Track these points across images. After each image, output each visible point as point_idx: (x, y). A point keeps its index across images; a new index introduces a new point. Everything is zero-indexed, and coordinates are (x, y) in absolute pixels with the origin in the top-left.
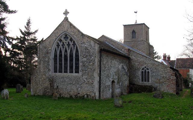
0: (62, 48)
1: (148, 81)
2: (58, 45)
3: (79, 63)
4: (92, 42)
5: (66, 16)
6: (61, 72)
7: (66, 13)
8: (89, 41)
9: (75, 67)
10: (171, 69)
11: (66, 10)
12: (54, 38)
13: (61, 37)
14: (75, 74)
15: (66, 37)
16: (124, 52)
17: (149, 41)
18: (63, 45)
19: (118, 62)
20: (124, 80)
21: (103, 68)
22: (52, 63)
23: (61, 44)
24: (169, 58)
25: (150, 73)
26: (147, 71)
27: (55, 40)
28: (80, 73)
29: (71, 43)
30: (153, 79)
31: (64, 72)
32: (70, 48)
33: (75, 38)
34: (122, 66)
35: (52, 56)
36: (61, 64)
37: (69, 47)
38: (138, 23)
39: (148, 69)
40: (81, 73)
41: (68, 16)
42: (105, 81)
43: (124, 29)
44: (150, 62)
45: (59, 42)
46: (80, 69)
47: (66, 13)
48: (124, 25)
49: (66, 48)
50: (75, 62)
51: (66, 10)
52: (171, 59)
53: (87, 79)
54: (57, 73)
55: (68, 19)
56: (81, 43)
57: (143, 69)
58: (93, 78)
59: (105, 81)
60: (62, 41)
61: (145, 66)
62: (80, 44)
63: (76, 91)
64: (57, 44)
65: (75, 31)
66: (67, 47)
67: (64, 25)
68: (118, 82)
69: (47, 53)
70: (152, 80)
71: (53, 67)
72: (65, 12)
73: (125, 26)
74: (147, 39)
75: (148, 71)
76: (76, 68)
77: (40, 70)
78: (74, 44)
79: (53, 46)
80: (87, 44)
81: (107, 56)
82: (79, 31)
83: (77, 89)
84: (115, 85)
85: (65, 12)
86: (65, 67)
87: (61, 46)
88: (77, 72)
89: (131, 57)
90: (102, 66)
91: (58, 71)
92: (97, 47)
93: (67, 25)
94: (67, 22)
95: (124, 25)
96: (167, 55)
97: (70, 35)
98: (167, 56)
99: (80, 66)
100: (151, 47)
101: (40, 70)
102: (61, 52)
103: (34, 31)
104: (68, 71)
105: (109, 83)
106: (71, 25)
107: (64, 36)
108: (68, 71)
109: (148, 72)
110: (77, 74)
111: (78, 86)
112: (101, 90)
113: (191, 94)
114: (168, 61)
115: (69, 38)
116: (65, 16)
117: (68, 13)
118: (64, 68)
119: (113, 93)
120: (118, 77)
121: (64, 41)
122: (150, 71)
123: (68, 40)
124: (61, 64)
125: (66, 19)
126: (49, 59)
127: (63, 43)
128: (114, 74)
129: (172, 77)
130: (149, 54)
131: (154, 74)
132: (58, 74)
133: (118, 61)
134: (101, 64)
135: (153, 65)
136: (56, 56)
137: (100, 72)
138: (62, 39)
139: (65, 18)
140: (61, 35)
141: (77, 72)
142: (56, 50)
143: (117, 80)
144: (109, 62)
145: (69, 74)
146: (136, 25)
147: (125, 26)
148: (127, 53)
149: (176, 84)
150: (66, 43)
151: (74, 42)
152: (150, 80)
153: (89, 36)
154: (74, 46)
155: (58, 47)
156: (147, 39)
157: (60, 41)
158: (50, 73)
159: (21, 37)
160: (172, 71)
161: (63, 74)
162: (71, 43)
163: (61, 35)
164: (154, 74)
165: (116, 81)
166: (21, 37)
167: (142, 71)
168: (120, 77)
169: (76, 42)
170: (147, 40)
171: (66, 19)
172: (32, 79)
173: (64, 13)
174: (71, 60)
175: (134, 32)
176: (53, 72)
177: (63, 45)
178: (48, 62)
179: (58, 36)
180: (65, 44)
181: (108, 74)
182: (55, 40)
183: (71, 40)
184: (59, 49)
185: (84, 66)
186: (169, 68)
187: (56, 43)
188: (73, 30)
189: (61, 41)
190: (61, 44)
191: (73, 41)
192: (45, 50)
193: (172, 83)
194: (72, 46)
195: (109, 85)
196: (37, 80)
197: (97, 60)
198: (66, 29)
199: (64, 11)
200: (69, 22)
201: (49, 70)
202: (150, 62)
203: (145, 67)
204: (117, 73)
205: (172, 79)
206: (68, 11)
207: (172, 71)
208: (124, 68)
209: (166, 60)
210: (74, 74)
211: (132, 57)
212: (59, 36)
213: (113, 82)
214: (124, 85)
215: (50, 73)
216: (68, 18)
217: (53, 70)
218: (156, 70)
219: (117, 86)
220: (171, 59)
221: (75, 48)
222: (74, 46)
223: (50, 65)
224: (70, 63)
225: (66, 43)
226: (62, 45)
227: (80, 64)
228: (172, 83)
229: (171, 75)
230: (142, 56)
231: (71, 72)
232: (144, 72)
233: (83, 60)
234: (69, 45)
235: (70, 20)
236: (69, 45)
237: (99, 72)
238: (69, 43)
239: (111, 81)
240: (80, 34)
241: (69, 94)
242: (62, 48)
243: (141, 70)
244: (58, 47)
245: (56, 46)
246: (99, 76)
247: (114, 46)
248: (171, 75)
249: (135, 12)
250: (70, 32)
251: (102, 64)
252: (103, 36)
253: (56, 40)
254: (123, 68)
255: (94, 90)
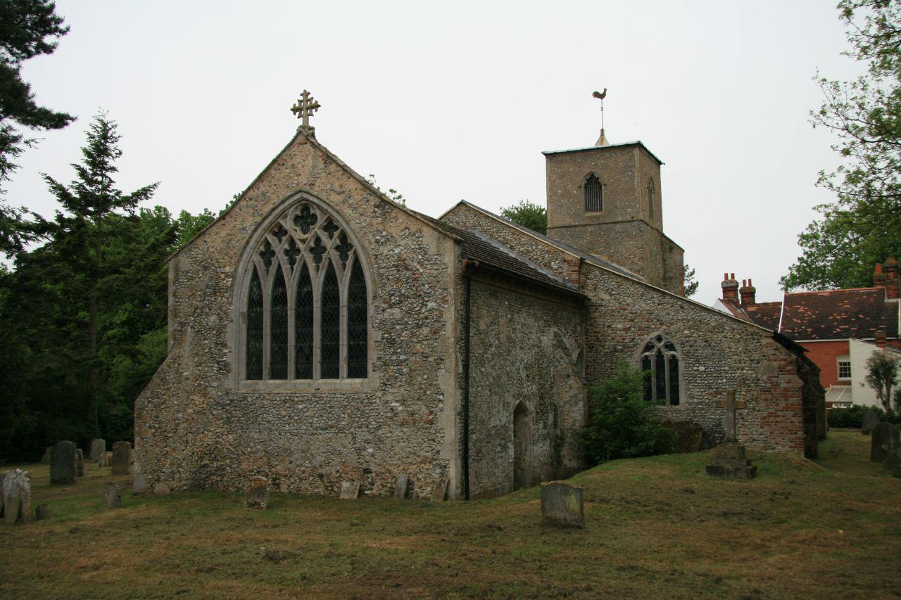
0: (288, 266)
1: (675, 401)
2: (267, 254)
3: (365, 332)
4: (427, 232)
5: (306, 121)
6: (279, 372)
7: (306, 106)
8: (413, 230)
9: (350, 348)
10: (778, 344)
11: (306, 94)
12: (249, 224)
13: (283, 215)
14: (350, 380)
15: (305, 218)
16: (558, 272)
17: (385, 206)
18: (292, 251)
19: (537, 320)
20: (565, 403)
21: (477, 351)
22: (236, 335)
23: (280, 247)
24: (749, 293)
25: (681, 365)
26: (667, 354)
27: (255, 231)
28: (374, 378)
29: (329, 243)
30: (696, 392)
31: (297, 377)
32: (325, 263)
33: (356, 223)
34: (556, 335)
35: (239, 303)
36: (279, 337)
37: (318, 259)
38: (613, 140)
39: (670, 347)
40: (378, 374)
41: (312, 122)
42: (485, 406)
43: (550, 172)
44: (681, 315)
45: (271, 238)
46: (372, 355)
47: (306, 106)
48: (547, 155)
49: (279, 266)
50: (349, 325)
51: (306, 94)
52: (759, 299)
53: (403, 402)
54: (260, 382)
55: (313, 135)
56: (377, 241)
57: (649, 347)
58: (432, 399)
59: (485, 406)
60: (286, 232)
61: (656, 334)
62: (370, 243)
63: (353, 458)
64: (262, 248)
65: (351, 185)
66: (309, 258)
67: (297, 160)
68: (541, 413)
69: (216, 291)
70: (692, 397)
71: (244, 356)
72: (300, 102)
73: (550, 157)
74: (651, 210)
75: (674, 356)
76: (351, 356)
77: (177, 371)
78: (344, 246)
79: (245, 256)
80: (402, 243)
81: (494, 295)
82: (366, 186)
83: (359, 451)
84: (526, 424)
85: (300, 102)
86: (299, 350)
87: (281, 258)
88: (358, 370)
89: (590, 295)
90: (474, 340)
91: (266, 371)
92: (450, 258)
93: (310, 161)
94: (308, 146)
95: (547, 155)
96: (739, 279)
97: (325, 207)
98: (741, 286)
99: (371, 343)
100: (671, 249)
101: (177, 371)
102: (280, 281)
103: (127, 193)
104: (317, 367)
105: (503, 418)
106: (329, 158)
107: (292, 213)
108: (317, 367)
109: (674, 361)
110: (358, 380)
111: (362, 435)
112: (472, 452)
113: (878, 454)
114: (744, 305)
115: (321, 221)
116: (300, 122)
117: (317, 106)
118: (297, 357)
119: (518, 461)
120: (542, 387)
121: (298, 235)
122: (679, 355)
123: (317, 229)
124: (279, 337)
125: (306, 135)
126: (223, 316)
127: (292, 242)
128: (523, 375)
129: (783, 380)
130: (665, 279)
131: (702, 368)
132: (267, 385)
133: (539, 314)
134: (468, 332)
135: (696, 326)
136: (255, 302)
137: (466, 367)
138: (288, 224)
139: (299, 133)
140: (281, 208)
141: (358, 370)
142: (255, 276)
143: (536, 401)
144: (502, 321)
145: (319, 383)
146: (603, 151)
147: (550, 157)
148: (574, 276)
149: (805, 411)
150: (303, 241)
151: (344, 237)
152: (683, 398)
153: (415, 212)
154: (344, 257)
155: (268, 263)
156: (651, 210)
157: (275, 234)
158: (229, 383)
159: (60, 218)
160: (784, 350)
161: (293, 385)
162: (329, 243)
163: (281, 208)
164: (702, 368)
165: (531, 406)
166: (60, 218)
167: (646, 357)
168: (547, 386)
169: (353, 239)
170: (651, 216)
171: (306, 135)
172: (140, 416)
173: (295, 110)
174: (330, 318)
175: (593, 184)
176: (244, 376)
177: (292, 251)
178: (220, 331)
179: (267, 209)
180: (301, 246)
181: (500, 377)
182: (255, 231)
183: (330, 226)
184: (273, 270)
185: (392, 342)
186: (771, 340)
187: (257, 242)
188: (337, 185)
189: (280, 232)
190: (280, 247)
191: (336, 234)
192: (204, 279)
193: (787, 408)
194: (335, 256)
195: (505, 427)
196: (165, 416)
197: (450, 315)
198: (304, 180)
199: (295, 100)
200: (317, 146)
201: (224, 368)
202: (681, 315)
203: (659, 339)
204: (538, 369)
205: (786, 389)
206: (316, 96)
207: (783, 354)
208: (564, 349)
209: (736, 303)
210: (346, 383)
211: (599, 295)
212: (273, 209)
213: (520, 411)
214: (568, 423)
215: (229, 383)
216: (313, 129)
217: (243, 369)
218: (708, 351)
219: (534, 427)
220: (759, 299)
221: (349, 262)
222: (344, 257)
223: (230, 343)
224: (324, 334)
225: (303, 241)
226: (337, 248)
227: (374, 335)
228: (787, 408)
229: (781, 370)
230: (641, 290)
231: (330, 371)
232: (653, 360)
233: (386, 315)
234: (318, 250)
235: (320, 138)
236: (318, 250)
237: (461, 370)
238: (318, 240)
239: (512, 409)
240: (374, 201)
241: (321, 476)
242: (286, 267)
243: (638, 354)
244: (268, 263)
245: (257, 259)
246: (463, 384)
247: (511, 248)
248: (781, 370)
249: (597, 95)
250: (325, 191)
251: (472, 331)
252: (462, 204)
253: (260, 231)
254: (560, 345)
255: (438, 452)
